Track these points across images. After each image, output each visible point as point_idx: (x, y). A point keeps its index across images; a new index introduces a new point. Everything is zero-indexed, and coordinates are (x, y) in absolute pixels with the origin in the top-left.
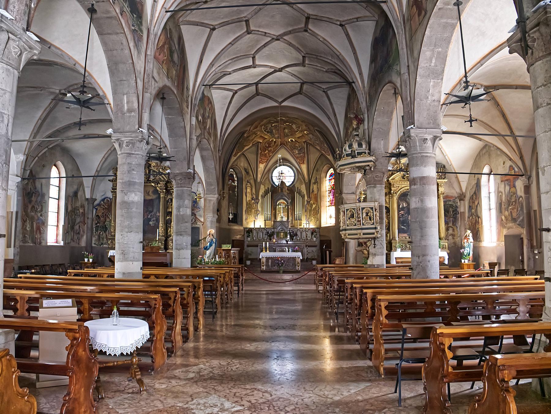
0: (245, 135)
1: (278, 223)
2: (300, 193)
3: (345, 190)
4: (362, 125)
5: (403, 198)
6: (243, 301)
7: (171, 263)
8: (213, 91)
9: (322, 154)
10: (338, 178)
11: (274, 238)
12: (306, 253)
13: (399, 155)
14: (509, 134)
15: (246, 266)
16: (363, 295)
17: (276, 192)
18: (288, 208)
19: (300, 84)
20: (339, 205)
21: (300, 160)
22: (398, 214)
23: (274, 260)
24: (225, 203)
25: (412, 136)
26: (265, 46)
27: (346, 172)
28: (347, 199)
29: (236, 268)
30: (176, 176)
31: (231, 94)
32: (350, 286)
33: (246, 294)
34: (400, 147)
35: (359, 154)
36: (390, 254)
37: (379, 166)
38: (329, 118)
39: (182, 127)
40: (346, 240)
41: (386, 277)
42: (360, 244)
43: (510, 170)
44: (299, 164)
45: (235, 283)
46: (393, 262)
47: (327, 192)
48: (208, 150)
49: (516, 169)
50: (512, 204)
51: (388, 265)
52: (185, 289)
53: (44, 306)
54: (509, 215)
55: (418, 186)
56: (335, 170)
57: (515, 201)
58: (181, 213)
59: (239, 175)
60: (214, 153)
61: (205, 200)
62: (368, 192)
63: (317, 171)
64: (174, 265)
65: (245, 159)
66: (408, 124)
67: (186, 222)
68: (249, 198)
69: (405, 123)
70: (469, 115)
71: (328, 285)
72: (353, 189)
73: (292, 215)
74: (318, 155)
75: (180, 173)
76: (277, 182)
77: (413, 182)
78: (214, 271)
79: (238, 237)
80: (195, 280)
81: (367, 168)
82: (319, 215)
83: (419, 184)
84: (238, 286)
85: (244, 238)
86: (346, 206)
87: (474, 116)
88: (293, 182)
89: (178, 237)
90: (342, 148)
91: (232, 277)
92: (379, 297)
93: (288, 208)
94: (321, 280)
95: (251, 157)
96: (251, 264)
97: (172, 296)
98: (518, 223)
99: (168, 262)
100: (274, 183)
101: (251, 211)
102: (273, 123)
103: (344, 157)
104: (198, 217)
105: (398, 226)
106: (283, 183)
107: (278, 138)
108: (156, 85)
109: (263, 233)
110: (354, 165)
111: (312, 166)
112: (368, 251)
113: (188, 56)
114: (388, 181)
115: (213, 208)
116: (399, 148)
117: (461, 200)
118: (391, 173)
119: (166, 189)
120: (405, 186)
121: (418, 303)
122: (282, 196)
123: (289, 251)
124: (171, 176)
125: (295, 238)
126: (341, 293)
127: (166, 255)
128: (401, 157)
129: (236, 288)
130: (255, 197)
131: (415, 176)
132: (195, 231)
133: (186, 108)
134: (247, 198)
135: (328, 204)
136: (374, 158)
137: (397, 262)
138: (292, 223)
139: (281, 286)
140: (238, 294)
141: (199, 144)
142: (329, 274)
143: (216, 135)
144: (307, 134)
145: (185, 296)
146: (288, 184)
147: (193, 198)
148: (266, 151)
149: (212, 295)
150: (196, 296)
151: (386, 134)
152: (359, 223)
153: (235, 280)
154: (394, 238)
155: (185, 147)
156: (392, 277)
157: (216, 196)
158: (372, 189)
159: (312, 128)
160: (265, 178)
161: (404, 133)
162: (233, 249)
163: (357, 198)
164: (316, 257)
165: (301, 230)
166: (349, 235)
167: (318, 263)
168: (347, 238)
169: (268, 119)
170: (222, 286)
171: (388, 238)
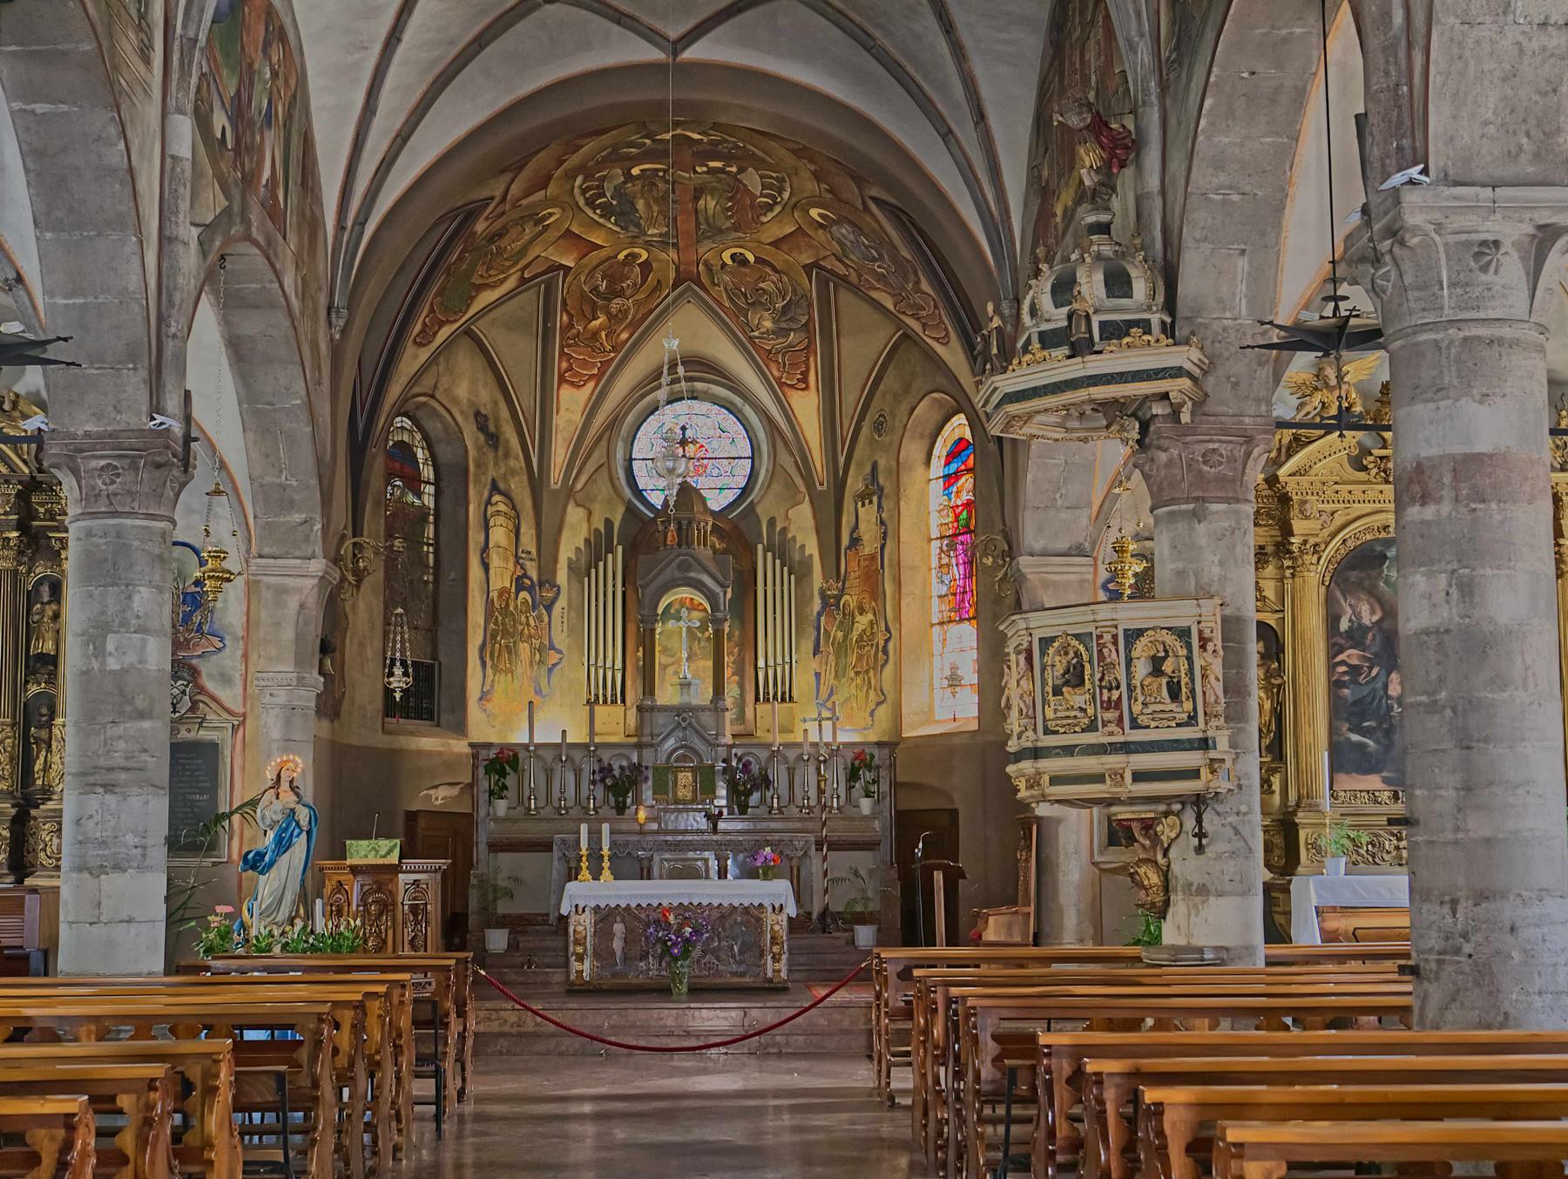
0: (480, 227)
1: (661, 719)
2: (782, 550)
3: (1032, 534)
4: (1129, 172)
5: (1354, 575)
6: (469, 1159)
7: (48, 954)
9: (908, 337)
10: (993, 463)
11: (638, 801)
12: (818, 884)
13: (1335, 338)
15: (483, 958)
16: (1138, 1115)
17: (647, 545)
18: (718, 634)
20: (997, 617)
21: (786, 370)
22: (1331, 668)
23: (649, 929)
24: (365, 608)
25: (1415, 230)
27: (1040, 428)
28: (1046, 585)
29: (424, 970)
30: (77, 450)
32: (1065, 1067)
33: (480, 1118)
34: (1343, 289)
35: (1114, 331)
36: (1286, 890)
37: (1223, 401)
38: (947, 134)
39: (112, 171)
40: (1042, 810)
41: (1269, 1017)
42: (1118, 834)
44: (779, 389)
45: (421, 1059)
46: (1306, 934)
47: (935, 545)
48: (272, 306)
51: (1279, 950)
52: (125, 1101)
53: (600, 710)
55: (1445, 508)
56: (975, 422)
58: (113, 664)
60: (305, 326)
61: (252, 588)
62: (1162, 547)
63: (879, 427)
64: (64, 962)
65: (480, 361)
66: (1391, 162)
67: (141, 715)
68: (501, 578)
69: (1375, 153)
71: (940, 1060)
72: (1080, 526)
73: (740, 671)
75: (100, 436)
77: (1413, 485)
78: (303, 991)
79: (440, 797)
80: (187, 1047)
81: (1158, 409)
82: (889, 668)
83: (1447, 493)
84: (438, 1075)
85: (475, 804)
86: (1041, 624)
88: (745, 491)
89: (93, 803)
90: (1018, 301)
91: (405, 1022)
92: (1235, 1133)
93: (718, 634)
94: (904, 1037)
95: (517, 352)
96: (513, 946)
97: (46, 1143)
99: (32, 944)
100: (638, 493)
101: (511, 651)
102: (637, 160)
103: (1026, 350)
104: (210, 685)
105: (1332, 731)
106: (687, 493)
107: (664, 245)
109: (578, 773)
110: (1081, 394)
111: (850, 398)
112: (1166, 874)
113: (323, 181)
114: (1272, 480)
115: (299, 637)
116: (1336, 299)
118: (1287, 435)
119: (22, 526)
120: (1371, 508)
121: (1458, 1169)
122: (685, 567)
123: (722, 874)
124: (53, 449)
125: (755, 798)
126: (1017, 1111)
127: (17, 907)
128: (1349, 347)
129: (426, 1087)
131: (1426, 452)
132: (192, 767)
134: (490, 575)
135: (937, 610)
136: (1195, 354)
137: (1329, 936)
138: (741, 717)
139: (688, 1073)
140: (438, 1118)
141: (216, 273)
142: (949, 1001)
143: (312, 225)
145: (127, 1141)
146: (717, 502)
147: (181, 576)
148: (589, 316)
149: (283, 1131)
150: (191, 1139)
151: (1263, 221)
152: (1111, 715)
153: (419, 1040)
154: (1306, 800)
155: (134, 282)
156: (1302, 1016)
157: (318, 566)
158: (1181, 526)
159: (850, 190)
161: (1365, 210)
162: (409, 863)
163: (1103, 575)
164: (872, 907)
165: (791, 754)
166: (1055, 780)
167: (883, 940)
168: (1043, 798)
169: (606, 139)
170: (344, 1077)
171: (1277, 799)
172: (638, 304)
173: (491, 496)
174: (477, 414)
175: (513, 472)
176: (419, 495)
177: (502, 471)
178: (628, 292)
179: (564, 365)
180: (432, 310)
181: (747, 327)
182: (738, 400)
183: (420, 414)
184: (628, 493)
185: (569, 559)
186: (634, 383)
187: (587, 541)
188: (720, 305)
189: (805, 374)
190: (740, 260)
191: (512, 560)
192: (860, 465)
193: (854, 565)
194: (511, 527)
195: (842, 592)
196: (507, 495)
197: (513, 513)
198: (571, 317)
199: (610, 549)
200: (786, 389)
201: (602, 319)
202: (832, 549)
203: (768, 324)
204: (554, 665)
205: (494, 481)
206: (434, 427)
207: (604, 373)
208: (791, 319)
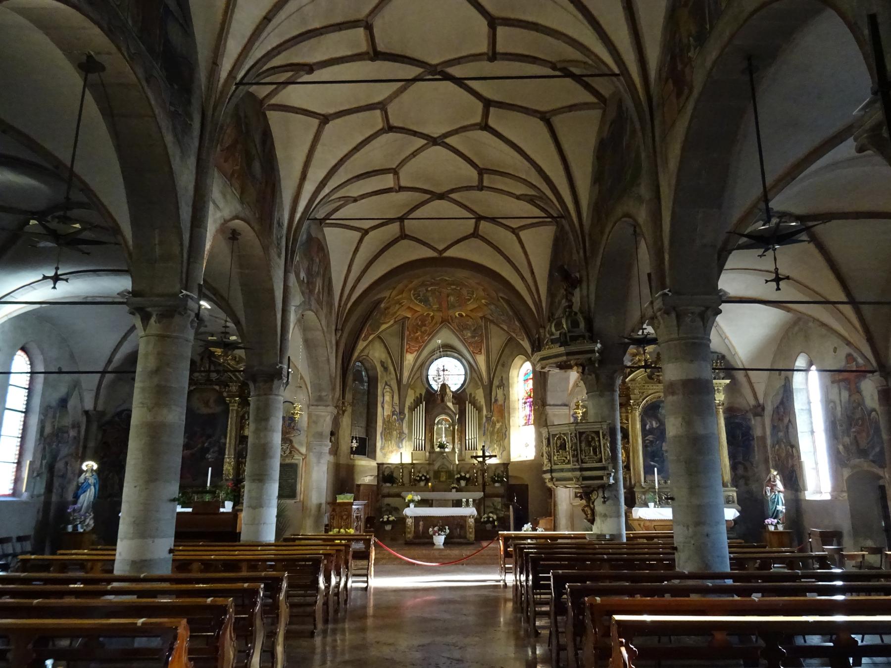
0: (383, 305)
2: (474, 403)
3: (550, 400)
8: (327, 230)
14: (845, 299)
17: (433, 401)
18: (454, 429)
19: (474, 220)
21: (475, 346)
22: (644, 441)
26: (414, 154)
31: (358, 235)
43: (848, 362)
44: (473, 354)
49: (860, 361)
50: (856, 424)
54: (851, 444)
57: (863, 419)
59: (370, 373)
68: (387, 412)
70: (772, 269)
73: (460, 440)
74: (504, 338)
76: (436, 386)
87: (783, 271)
88: (463, 385)
95: (394, 342)
98: (871, 458)
100: (430, 385)
101: (390, 434)
104: (296, 446)
106: (444, 386)
108: (219, 215)
111: (494, 356)
116: (643, 329)
117: (756, 415)
133: (276, 257)
134: (384, 410)
144: (486, 305)
148: (416, 333)
160: (416, 377)
190: (461, 315)
201: (419, 333)
203: (469, 335)
206: (366, 365)
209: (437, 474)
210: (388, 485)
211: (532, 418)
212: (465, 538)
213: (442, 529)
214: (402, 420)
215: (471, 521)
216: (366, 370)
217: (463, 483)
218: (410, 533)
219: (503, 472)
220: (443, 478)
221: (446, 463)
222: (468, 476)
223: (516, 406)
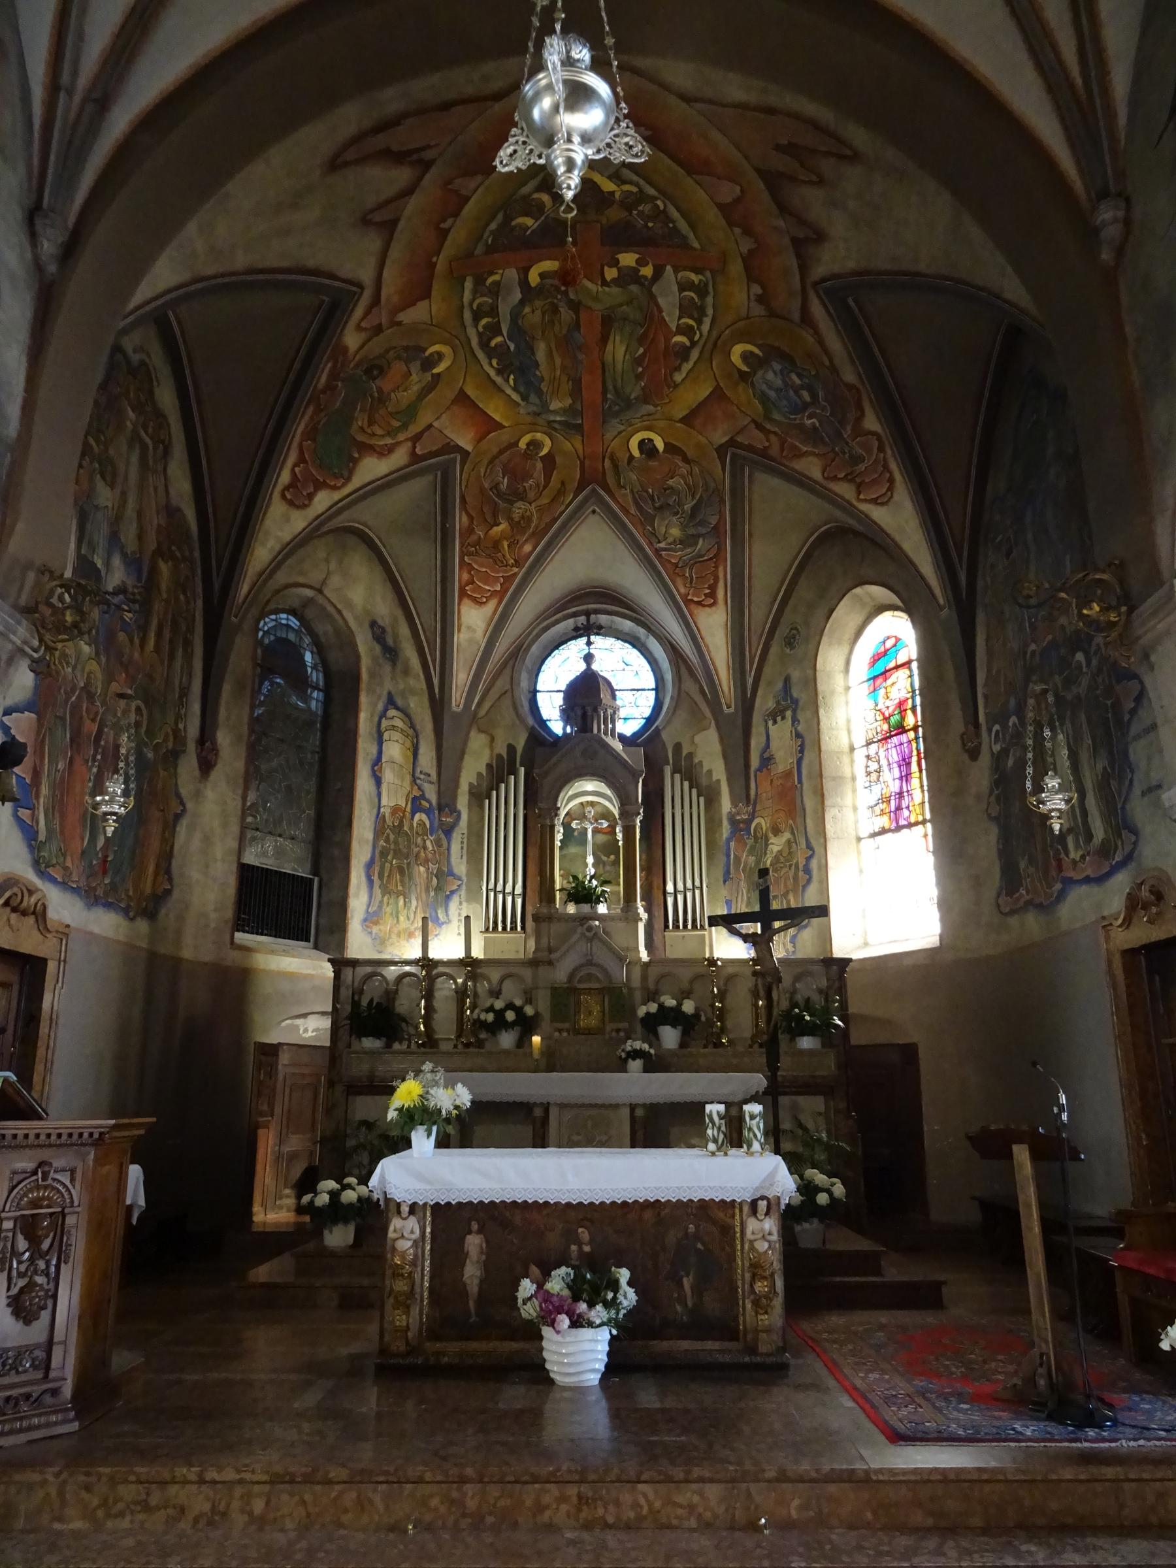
2: (689, 772)
21: (690, 581)
44: (683, 610)
59: (333, 656)
65: (378, 573)
68: (394, 795)
88: (650, 721)
95: (416, 558)
111: (758, 612)
130: (433, 797)
134: (382, 787)
148: (486, 517)
172: (540, 509)
173: (386, 710)
174: (373, 624)
175: (412, 692)
176: (306, 699)
177: (401, 686)
178: (531, 495)
179: (465, 576)
180: (302, 459)
181: (653, 537)
182: (641, 632)
183: (309, 613)
184: (531, 721)
185: (470, 784)
186: (541, 608)
187: (489, 766)
188: (626, 511)
189: (713, 588)
190: (647, 447)
191: (408, 778)
192: (770, 683)
193: (765, 786)
194: (409, 744)
195: (753, 816)
196: (406, 713)
197: (411, 732)
198: (471, 518)
199: (514, 772)
200: (692, 606)
201: (503, 526)
202: (740, 771)
203: (675, 532)
204: (453, 892)
205: (389, 694)
206: (322, 628)
207: (506, 591)
208: (702, 523)
209: (565, 999)
210: (369, 1043)
211: (918, 793)
212: (728, 1330)
213: (592, 1287)
214: (448, 831)
215: (763, 1231)
216: (320, 649)
217: (670, 1036)
218: (405, 1302)
219: (825, 993)
220: (589, 1019)
221: (601, 956)
222: (688, 1007)
223: (847, 772)
